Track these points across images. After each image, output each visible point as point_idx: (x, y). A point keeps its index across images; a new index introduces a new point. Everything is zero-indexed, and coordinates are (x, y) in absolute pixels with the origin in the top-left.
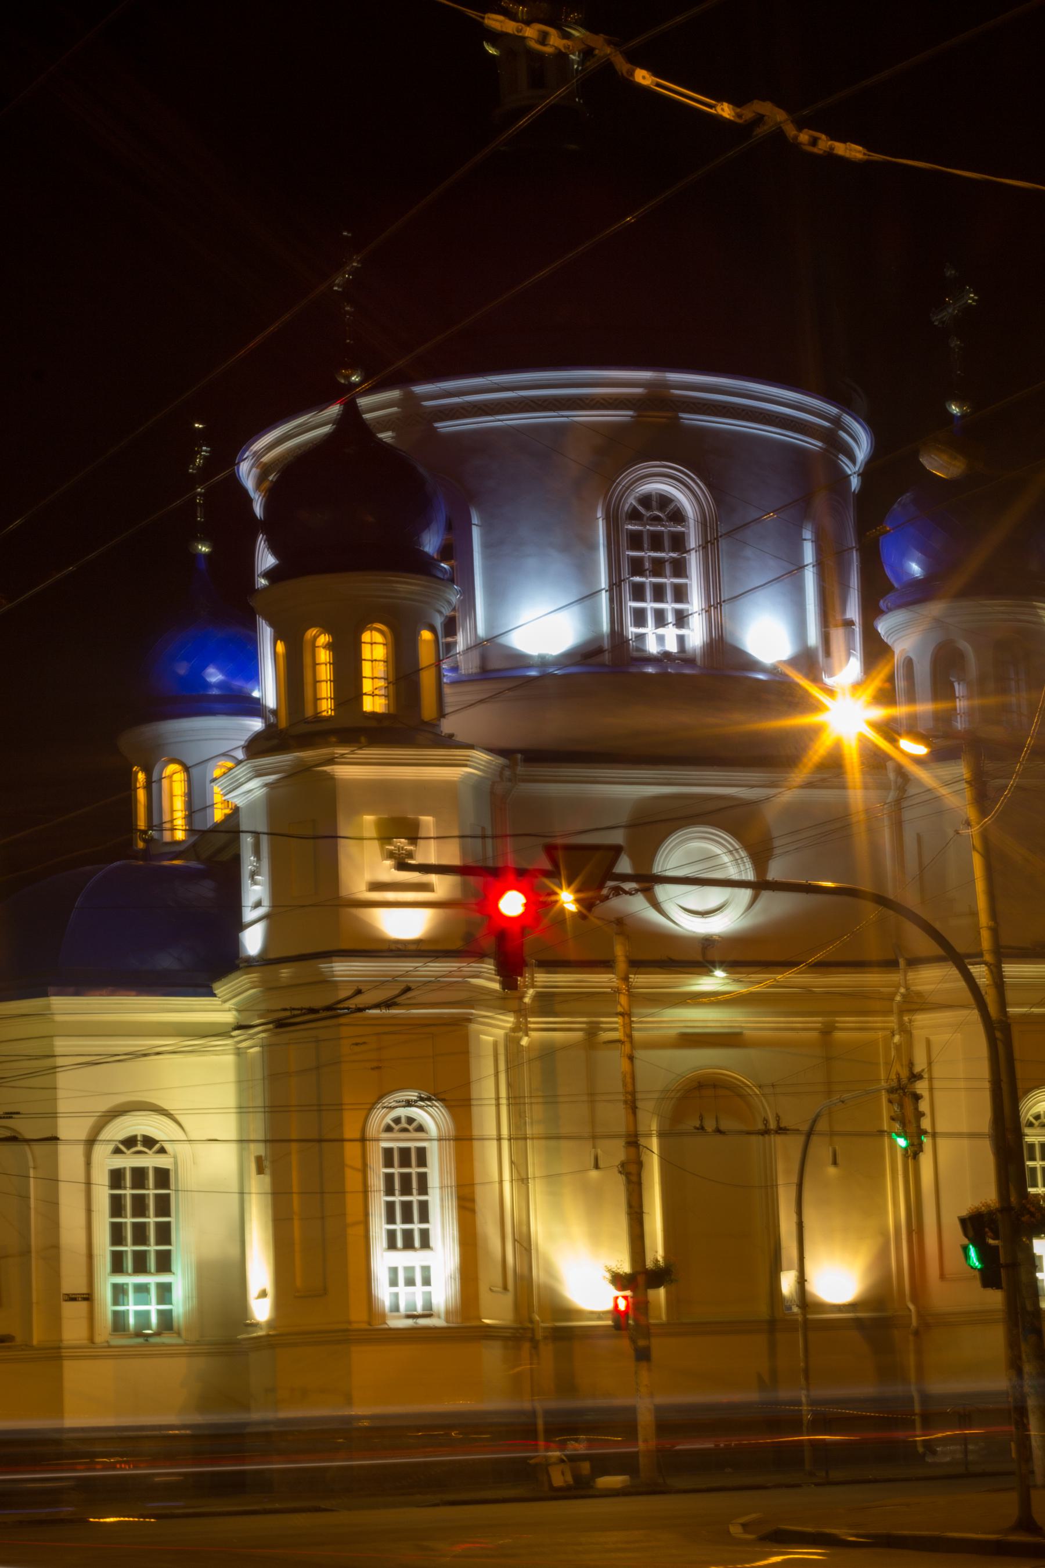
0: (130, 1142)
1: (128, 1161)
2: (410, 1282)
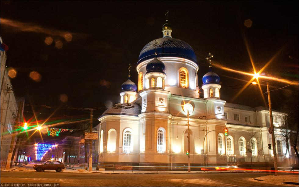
0: (127, 131)
1: (127, 133)
2: (160, 148)
